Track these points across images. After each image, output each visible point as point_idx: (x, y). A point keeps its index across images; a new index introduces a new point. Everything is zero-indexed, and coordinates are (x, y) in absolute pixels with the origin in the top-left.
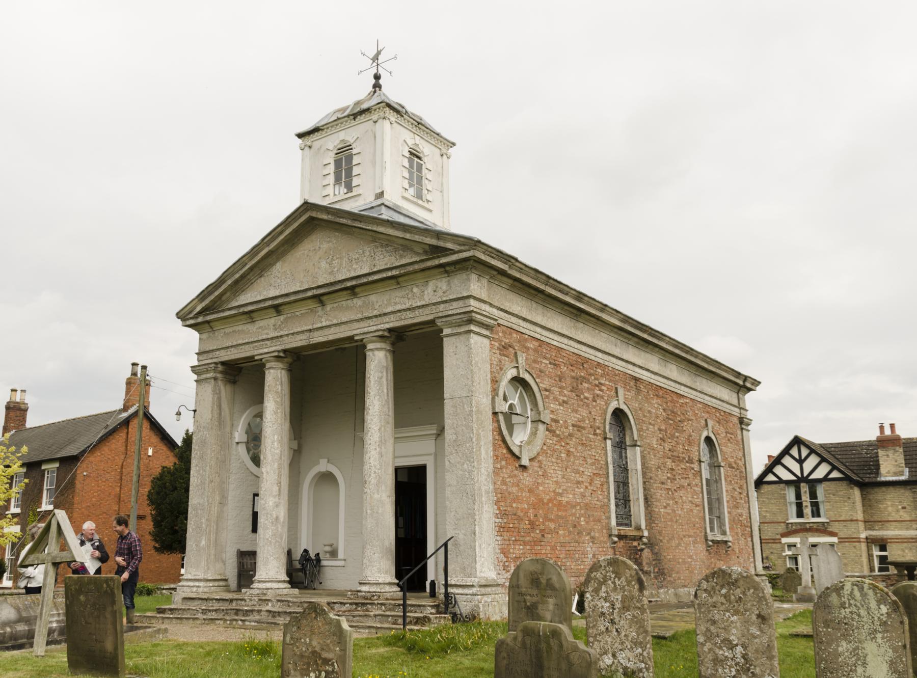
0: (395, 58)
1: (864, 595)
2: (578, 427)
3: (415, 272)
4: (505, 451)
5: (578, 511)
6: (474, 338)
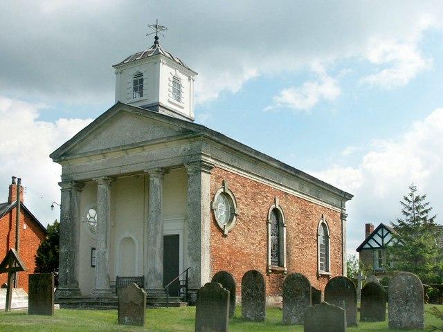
2: (254, 217)
5: (252, 257)
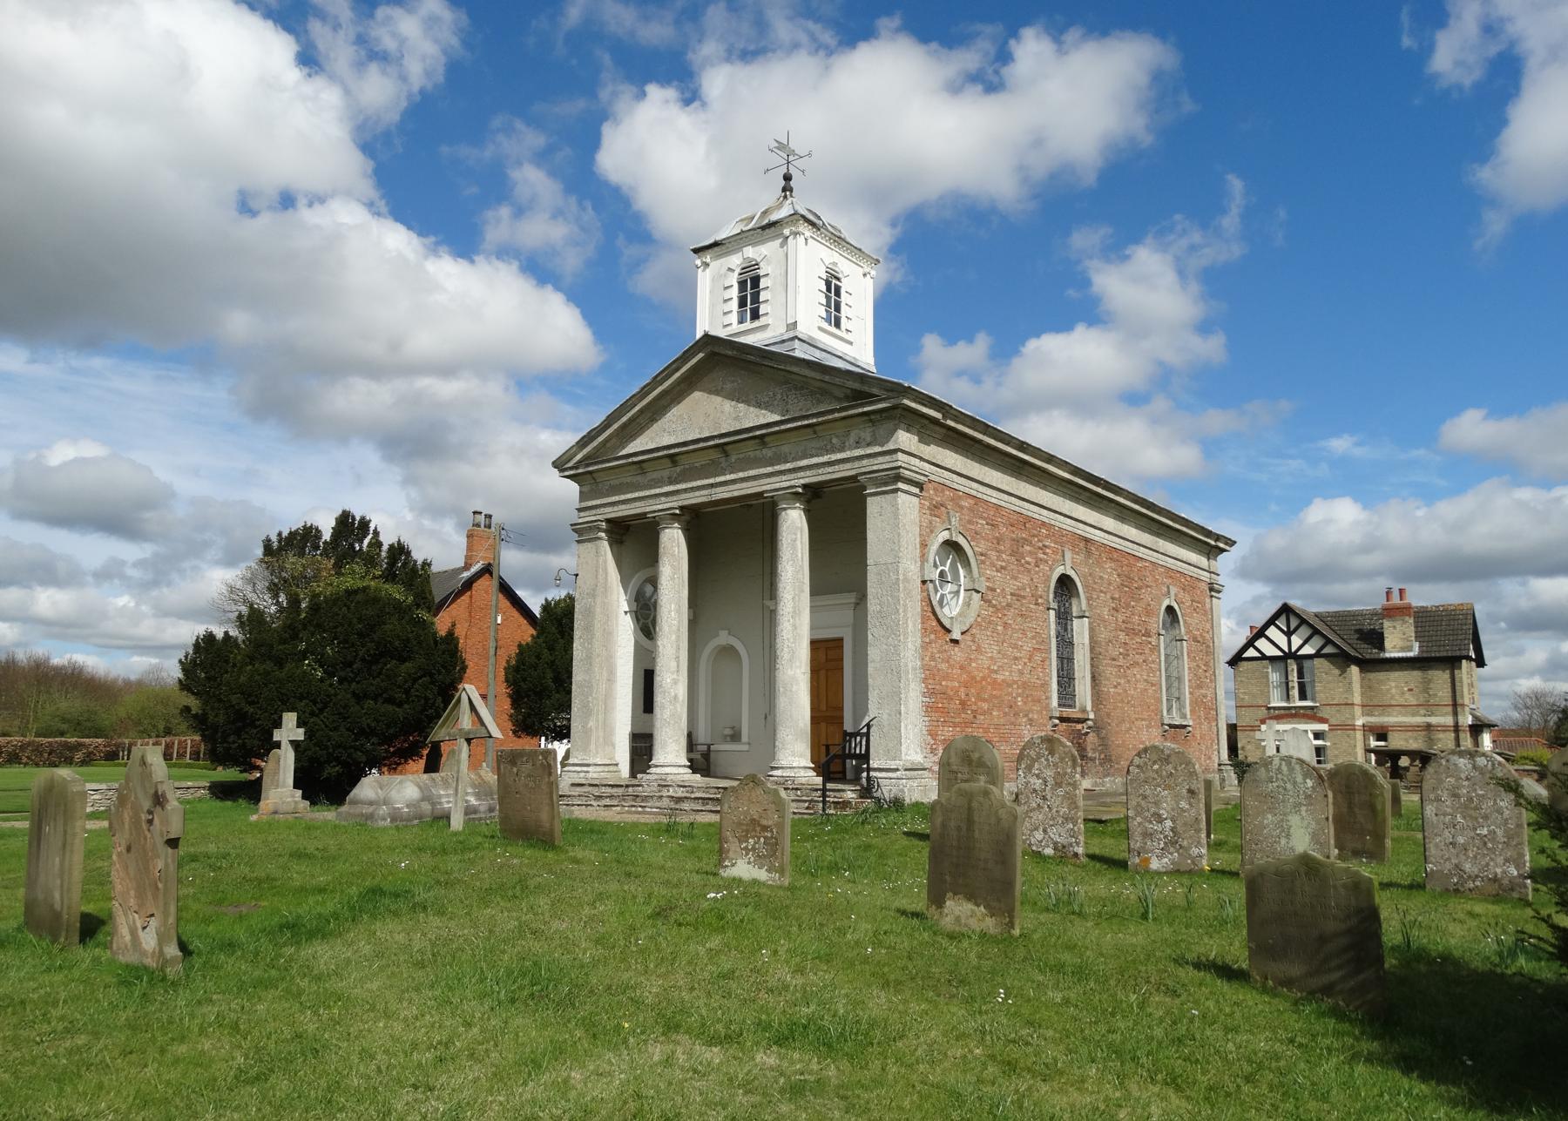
0: (809, 154)
1: (1291, 770)
2: (1017, 596)
3: (836, 420)
4: (934, 623)
5: (1015, 690)
6: (901, 496)
